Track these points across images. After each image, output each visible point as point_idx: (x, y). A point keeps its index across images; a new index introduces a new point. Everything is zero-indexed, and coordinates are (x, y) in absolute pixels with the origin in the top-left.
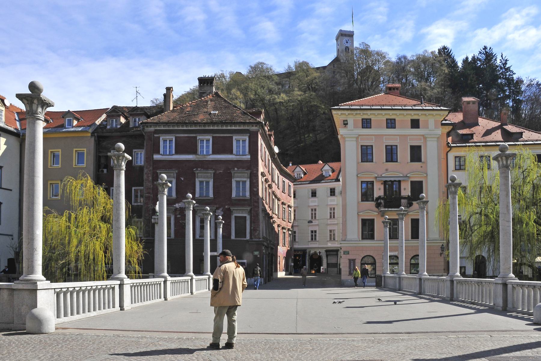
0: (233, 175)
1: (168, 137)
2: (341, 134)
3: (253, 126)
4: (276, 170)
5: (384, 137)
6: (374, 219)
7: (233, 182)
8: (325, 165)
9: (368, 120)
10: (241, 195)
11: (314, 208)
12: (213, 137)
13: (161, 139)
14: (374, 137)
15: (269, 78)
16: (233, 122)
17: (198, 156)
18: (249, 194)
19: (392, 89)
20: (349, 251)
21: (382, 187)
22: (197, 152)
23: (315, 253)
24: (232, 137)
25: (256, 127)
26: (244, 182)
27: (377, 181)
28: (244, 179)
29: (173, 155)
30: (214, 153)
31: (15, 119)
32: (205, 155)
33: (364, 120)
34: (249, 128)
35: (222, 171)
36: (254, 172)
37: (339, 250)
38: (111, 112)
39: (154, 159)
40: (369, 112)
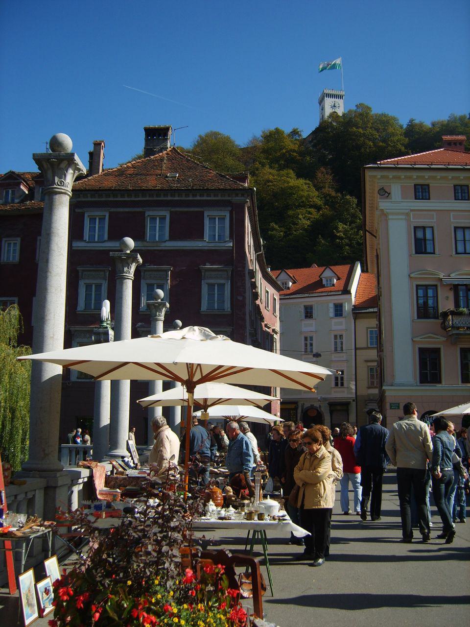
0: (203, 274)
1: (98, 213)
2: (381, 208)
3: (237, 195)
4: (260, 272)
5: (452, 214)
6: (440, 349)
7: (203, 286)
8: (325, 269)
9: (424, 187)
10: (216, 307)
12: (172, 213)
13: (86, 215)
14: (435, 213)
15: (232, 154)
16: (205, 188)
17: (146, 244)
18: (229, 306)
19: (452, 143)
20: (399, 404)
21: (451, 295)
22: (144, 238)
23: (312, 407)
24: (203, 213)
25: (241, 197)
26: (221, 286)
27: (442, 285)
28: (222, 281)
29: (105, 241)
30: (173, 237)
31: (86, 536)
32: (157, 242)
33: (417, 187)
34: (230, 198)
35: (184, 268)
36: (239, 269)
37: (350, 402)
38: (5, 178)
39: (73, 248)
40: (427, 174)
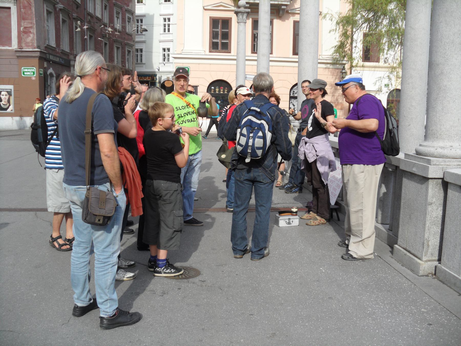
11: (167, 17)
